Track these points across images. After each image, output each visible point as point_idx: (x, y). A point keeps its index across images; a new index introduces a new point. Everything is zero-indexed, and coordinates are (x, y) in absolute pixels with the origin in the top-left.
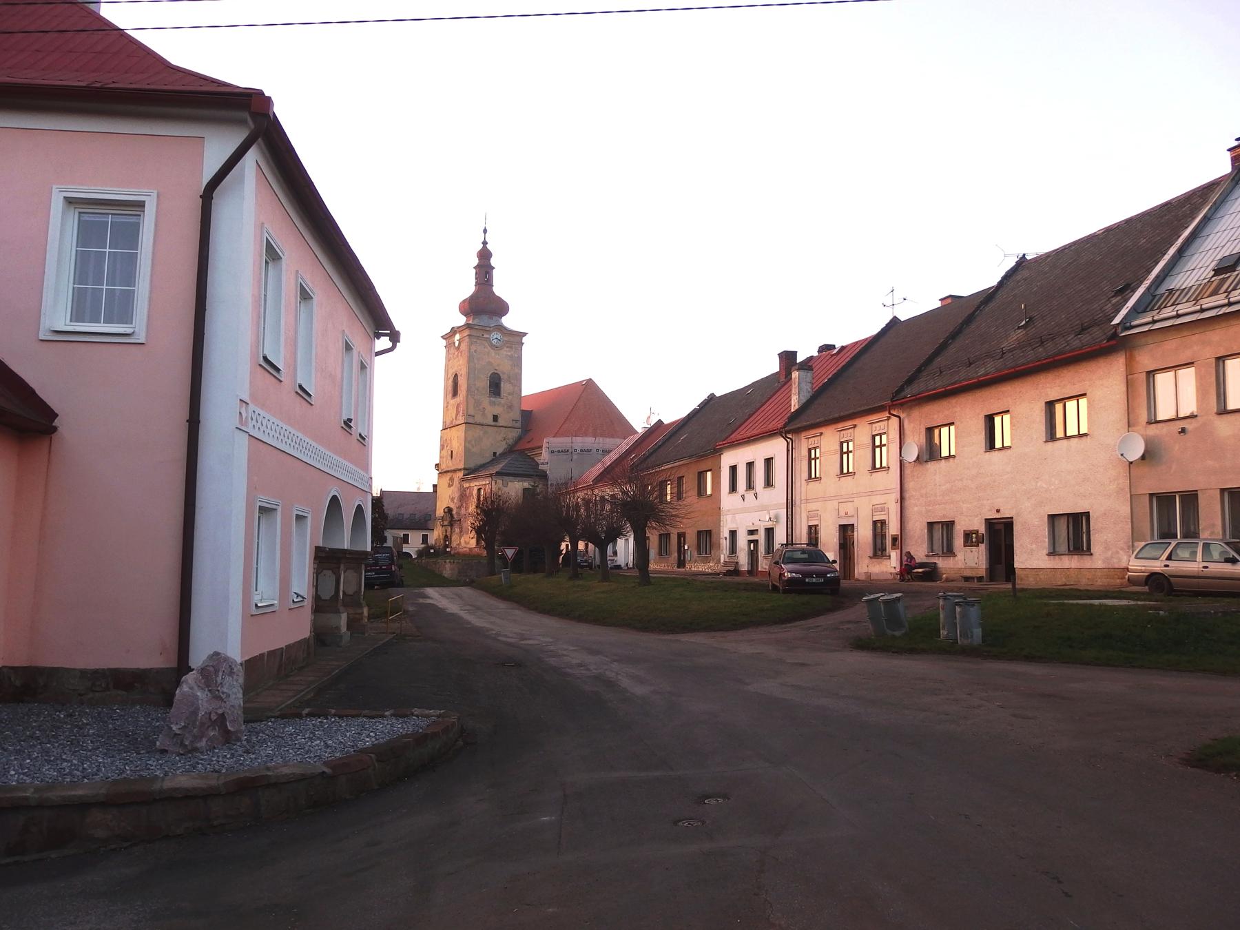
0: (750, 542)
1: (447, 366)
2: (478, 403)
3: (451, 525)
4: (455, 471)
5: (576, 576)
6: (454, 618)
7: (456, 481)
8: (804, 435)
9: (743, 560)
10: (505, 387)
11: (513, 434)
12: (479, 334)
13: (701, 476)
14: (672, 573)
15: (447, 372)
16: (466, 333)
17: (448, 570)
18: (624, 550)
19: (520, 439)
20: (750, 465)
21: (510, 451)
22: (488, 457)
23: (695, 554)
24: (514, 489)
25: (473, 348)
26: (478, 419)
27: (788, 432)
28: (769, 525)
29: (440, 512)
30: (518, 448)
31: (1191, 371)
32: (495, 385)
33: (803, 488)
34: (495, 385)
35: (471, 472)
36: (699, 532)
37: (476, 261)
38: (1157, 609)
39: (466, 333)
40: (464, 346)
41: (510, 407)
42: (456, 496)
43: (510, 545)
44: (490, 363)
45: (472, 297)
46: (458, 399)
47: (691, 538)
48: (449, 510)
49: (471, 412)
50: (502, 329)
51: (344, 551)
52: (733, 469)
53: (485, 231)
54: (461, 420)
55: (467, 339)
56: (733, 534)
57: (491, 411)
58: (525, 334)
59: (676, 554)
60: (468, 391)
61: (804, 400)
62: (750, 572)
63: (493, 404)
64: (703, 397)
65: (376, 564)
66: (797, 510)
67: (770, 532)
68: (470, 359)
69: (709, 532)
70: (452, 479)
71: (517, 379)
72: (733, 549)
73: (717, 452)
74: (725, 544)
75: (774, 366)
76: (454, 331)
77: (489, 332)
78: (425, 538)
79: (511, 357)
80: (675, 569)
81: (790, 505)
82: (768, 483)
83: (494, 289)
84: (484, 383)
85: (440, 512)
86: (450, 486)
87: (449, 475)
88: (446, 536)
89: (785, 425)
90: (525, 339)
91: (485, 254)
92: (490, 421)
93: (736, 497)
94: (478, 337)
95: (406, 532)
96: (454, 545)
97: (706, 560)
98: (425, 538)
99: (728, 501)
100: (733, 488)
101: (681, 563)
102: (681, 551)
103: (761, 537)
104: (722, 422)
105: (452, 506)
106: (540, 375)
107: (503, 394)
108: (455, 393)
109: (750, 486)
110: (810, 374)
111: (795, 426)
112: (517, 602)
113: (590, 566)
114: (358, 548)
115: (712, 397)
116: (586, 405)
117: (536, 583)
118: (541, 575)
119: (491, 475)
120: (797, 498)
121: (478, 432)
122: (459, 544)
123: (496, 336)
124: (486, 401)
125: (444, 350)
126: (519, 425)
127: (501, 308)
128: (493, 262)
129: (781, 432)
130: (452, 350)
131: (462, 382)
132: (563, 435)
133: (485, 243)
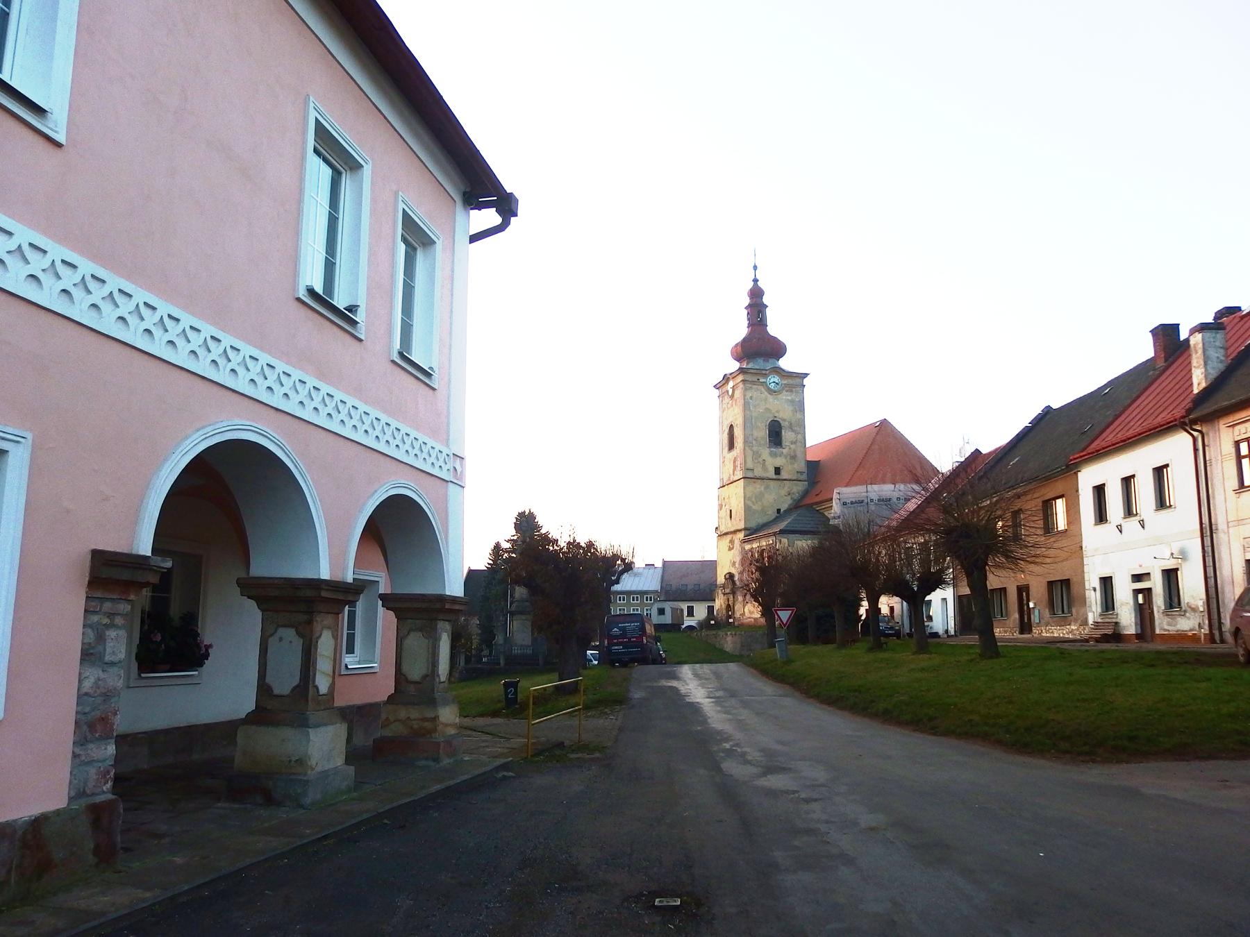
0: (1137, 592)
1: (721, 417)
2: (756, 455)
3: (733, 593)
4: (735, 532)
5: (878, 646)
6: (695, 708)
7: (737, 543)
8: (1222, 424)
9: (1127, 618)
10: (787, 436)
11: (799, 488)
13: (1048, 506)
14: (1015, 640)
15: (721, 423)
16: (740, 378)
17: (729, 642)
18: (942, 606)
19: (806, 493)
20: (1127, 481)
21: (796, 506)
22: (772, 514)
23: (1047, 613)
24: (803, 544)
25: (749, 394)
26: (759, 472)
27: (1194, 422)
28: (1170, 564)
29: (721, 579)
30: (808, 501)
32: (775, 434)
33: (1226, 503)
34: (775, 434)
35: (751, 532)
36: (1051, 584)
37: (747, 301)
39: (740, 378)
40: (738, 393)
41: (793, 458)
42: (738, 559)
43: (785, 606)
44: (767, 410)
45: (744, 340)
47: (1038, 591)
48: (730, 576)
49: (750, 465)
50: (779, 371)
51: (317, 584)
52: (1100, 491)
53: (755, 268)
54: (739, 475)
55: (741, 385)
56: (1107, 582)
57: (772, 463)
59: (1017, 616)
60: (745, 442)
61: (1214, 374)
62: (1139, 637)
63: (773, 455)
64: (1037, 410)
65: (624, 635)
66: (1221, 537)
67: (1171, 576)
68: (746, 406)
69: (1066, 583)
70: (732, 542)
71: (799, 427)
72: (1108, 602)
73: (1071, 469)
74: (1094, 598)
75: (1145, 350)
76: (726, 379)
77: (765, 376)
78: (711, 609)
79: (792, 401)
80: (1017, 635)
81: (1208, 532)
82: (1162, 503)
83: (769, 329)
84: (763, 433)
85: (721, 579)
86: (730, 549)
87: (729, 537)
89: (1189, 411)
90: (806, 381)
91: (756, 294)
92: (771, 474)
93: (1108, 529)
94: (753, 383)
95: (690, 604)
96: (737, 615)
97: (1064, 622)
98: (711, 609)
99: (1092, 535)
100: (1101, 517)
101: (1025, 627)
102: (1024, 611)
103: (1156, 584)
104: (1063, 440)
105: (733, 571)
106: (826, 422)
107: (784, 443)
108: (731, 446)
109: (1129, 512)
110: (1220, 335)
111: (1199, 414)
112: (792, 685)
113: (898, 634)
114: (338, 577)
115: (1048, 411)
116: (882, 448)
117: (824, 659)
118: (830, 647)
119: (775, 534)
120: (1220, 520)
121: (758, 487)
122: (743, 614)
123: (773, 379)
124: (765, 453)
125: (717, 401)
126: (804, 477)
127: (777, 349)
128: (765, 300)
129: (1183, 424)
130: (727, 399)
131: (738, 433)
132: (856, 484)
133: (755, 281)
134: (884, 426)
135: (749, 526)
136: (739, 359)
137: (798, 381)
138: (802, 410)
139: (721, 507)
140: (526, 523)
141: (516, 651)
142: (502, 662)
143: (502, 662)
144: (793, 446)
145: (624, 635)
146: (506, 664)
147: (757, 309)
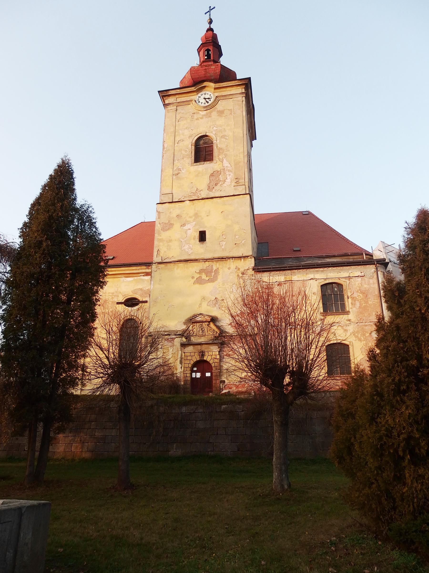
53: (211, 22)
87: (196, 267)
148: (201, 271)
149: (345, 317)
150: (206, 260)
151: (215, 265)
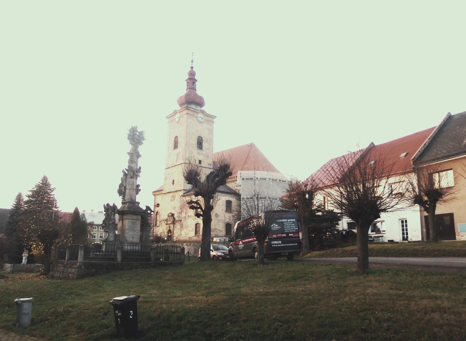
3: (174, 223)
10: (205, 145)
12: (192, 113)
31: (452, 171)
32: (200, 144)
37: (187, 77)
38: (81, 254)
45: (187, 95)
46: (177, 151)
50: (203, 112)
53: (192, 61)
55: (186, 116)
58: (215, 117)
63: (199, 154)
70: (173, 197)
71: (210, 142)
86: (172, 200)
87: (172, 194)
88: (169, 231)
90: (215, 120)
122: (181, 235)
126: (212, 167)
133: (192, 68)
134: (251, 146)
135: (185, 189)
136: (181, 105)
137: (211, 119)
138: (212, 134)
139: (166, 179)
140: (128, 153)
141: (127, 248)
142: (119, 257)
143: (119, 257)
144: (207, 151)
145: (282, 231)
146: (122, 260)
147: (192, 80)
148: (172, 196)
149: (186, 249)
150: (173, 192)
151: (175, 194)
